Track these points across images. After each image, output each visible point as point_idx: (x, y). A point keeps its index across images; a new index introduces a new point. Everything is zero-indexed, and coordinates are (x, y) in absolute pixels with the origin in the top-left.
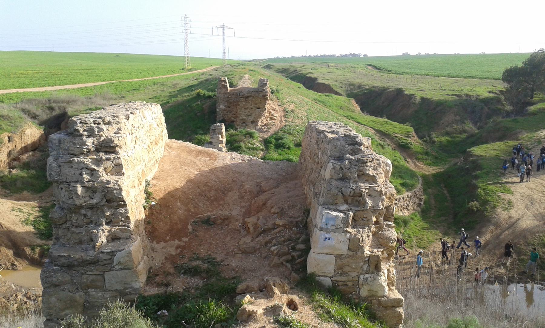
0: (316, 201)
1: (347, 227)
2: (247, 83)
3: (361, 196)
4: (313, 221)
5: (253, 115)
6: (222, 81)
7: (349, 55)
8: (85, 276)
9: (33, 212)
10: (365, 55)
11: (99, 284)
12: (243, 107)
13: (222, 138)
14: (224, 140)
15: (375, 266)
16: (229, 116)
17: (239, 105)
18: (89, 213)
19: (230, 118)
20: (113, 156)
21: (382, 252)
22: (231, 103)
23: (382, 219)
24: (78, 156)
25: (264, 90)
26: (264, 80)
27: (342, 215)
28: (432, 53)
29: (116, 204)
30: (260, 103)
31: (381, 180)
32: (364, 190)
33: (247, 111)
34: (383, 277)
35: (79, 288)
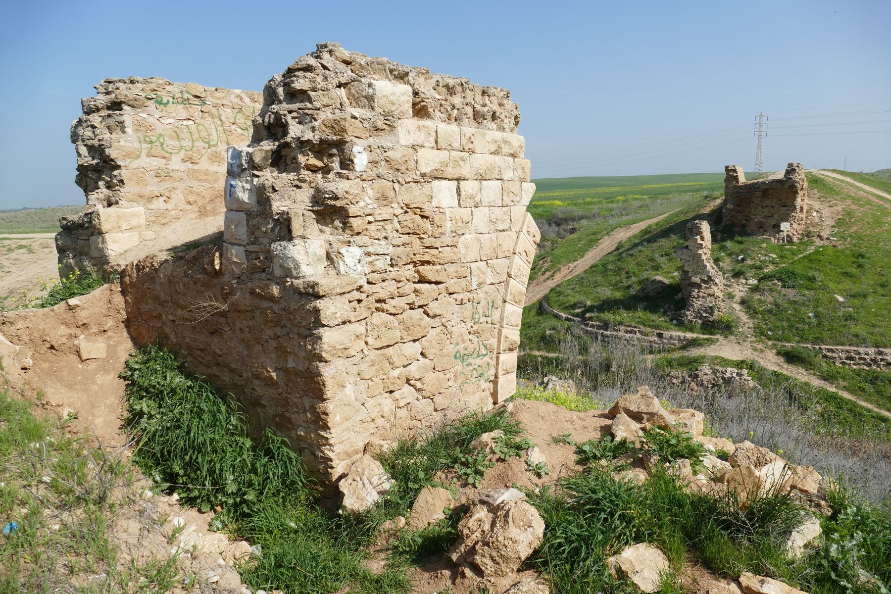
5: (776, 216)
13: (702, 239)
17: (753, 202)
33: (766, 211)
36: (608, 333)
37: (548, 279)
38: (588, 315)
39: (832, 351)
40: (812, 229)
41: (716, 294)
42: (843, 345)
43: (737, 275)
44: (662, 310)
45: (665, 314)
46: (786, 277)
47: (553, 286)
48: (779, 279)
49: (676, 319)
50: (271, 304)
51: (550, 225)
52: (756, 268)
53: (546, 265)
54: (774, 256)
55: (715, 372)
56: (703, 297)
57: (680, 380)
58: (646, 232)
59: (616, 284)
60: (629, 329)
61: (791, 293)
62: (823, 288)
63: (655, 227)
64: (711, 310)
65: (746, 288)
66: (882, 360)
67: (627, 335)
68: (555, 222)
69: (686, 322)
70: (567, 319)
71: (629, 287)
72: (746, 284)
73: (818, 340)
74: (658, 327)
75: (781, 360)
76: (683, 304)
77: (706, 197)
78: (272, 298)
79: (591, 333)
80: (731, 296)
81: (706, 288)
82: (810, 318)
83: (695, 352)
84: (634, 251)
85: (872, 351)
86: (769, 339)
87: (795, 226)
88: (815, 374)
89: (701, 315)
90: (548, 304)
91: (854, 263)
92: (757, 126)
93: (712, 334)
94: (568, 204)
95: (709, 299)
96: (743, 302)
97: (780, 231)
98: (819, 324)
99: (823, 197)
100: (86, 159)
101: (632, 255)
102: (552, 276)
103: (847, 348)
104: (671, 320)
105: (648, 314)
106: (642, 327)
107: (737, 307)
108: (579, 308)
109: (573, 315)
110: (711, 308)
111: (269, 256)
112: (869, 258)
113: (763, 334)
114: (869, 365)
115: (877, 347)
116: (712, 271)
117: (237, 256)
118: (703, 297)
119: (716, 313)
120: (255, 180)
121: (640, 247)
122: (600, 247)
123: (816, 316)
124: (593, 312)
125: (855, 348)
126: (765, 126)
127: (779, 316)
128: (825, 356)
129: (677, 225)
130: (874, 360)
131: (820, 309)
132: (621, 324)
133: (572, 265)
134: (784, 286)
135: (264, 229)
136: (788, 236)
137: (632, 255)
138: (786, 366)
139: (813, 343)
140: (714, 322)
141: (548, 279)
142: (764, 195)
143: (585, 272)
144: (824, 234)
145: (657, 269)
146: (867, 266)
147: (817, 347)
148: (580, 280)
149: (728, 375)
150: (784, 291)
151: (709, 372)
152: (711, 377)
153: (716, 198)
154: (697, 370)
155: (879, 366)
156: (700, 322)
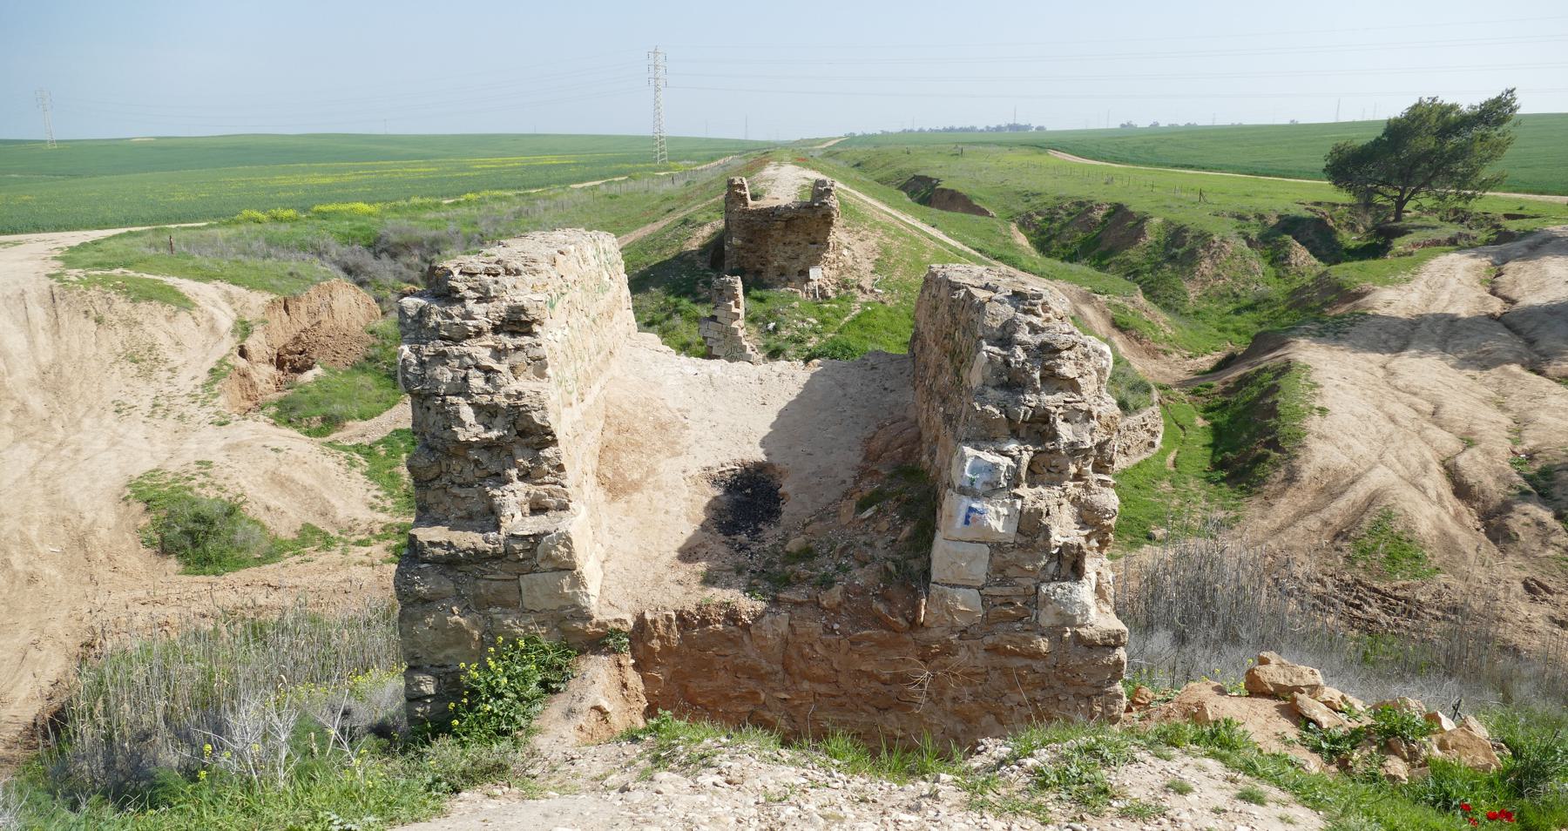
0: (949, 432)
1: (1017, 486)
2: (783, 187)
3: (1046, 421)
4: (944, 474)
5: (802, 258)
8: (481, 583)
10: (1039, 128)
11: (511, 598)
13: (737, 305)
14: (741, 311)
15: (1071, 565)
18: (484, 458)
20: (526, 340)
21: (1088, 538)
23: (1090, 468)
24: (457, 342)
26: (824, 182)
27: (1008, 461)
28: (1287, 122)
29: (536, 440)
31: (1089, 385)
32: (1053, 409)
33: (788, 249)
34: (1087, 588)
35: (472, 607)
40: (847, 276)
50: (1029, 662)
77: (685, 222)
78: (1036, 655)
87: (827, 270)
97: (808, 280)
100: (475, 430)
111: (1034, 600)
117: (963, 603)
120: (1019, 503)
126: (662, 71)
129: (653, 269)
135: (1030, 567)
144: (867, 283)
153: (701, 225)
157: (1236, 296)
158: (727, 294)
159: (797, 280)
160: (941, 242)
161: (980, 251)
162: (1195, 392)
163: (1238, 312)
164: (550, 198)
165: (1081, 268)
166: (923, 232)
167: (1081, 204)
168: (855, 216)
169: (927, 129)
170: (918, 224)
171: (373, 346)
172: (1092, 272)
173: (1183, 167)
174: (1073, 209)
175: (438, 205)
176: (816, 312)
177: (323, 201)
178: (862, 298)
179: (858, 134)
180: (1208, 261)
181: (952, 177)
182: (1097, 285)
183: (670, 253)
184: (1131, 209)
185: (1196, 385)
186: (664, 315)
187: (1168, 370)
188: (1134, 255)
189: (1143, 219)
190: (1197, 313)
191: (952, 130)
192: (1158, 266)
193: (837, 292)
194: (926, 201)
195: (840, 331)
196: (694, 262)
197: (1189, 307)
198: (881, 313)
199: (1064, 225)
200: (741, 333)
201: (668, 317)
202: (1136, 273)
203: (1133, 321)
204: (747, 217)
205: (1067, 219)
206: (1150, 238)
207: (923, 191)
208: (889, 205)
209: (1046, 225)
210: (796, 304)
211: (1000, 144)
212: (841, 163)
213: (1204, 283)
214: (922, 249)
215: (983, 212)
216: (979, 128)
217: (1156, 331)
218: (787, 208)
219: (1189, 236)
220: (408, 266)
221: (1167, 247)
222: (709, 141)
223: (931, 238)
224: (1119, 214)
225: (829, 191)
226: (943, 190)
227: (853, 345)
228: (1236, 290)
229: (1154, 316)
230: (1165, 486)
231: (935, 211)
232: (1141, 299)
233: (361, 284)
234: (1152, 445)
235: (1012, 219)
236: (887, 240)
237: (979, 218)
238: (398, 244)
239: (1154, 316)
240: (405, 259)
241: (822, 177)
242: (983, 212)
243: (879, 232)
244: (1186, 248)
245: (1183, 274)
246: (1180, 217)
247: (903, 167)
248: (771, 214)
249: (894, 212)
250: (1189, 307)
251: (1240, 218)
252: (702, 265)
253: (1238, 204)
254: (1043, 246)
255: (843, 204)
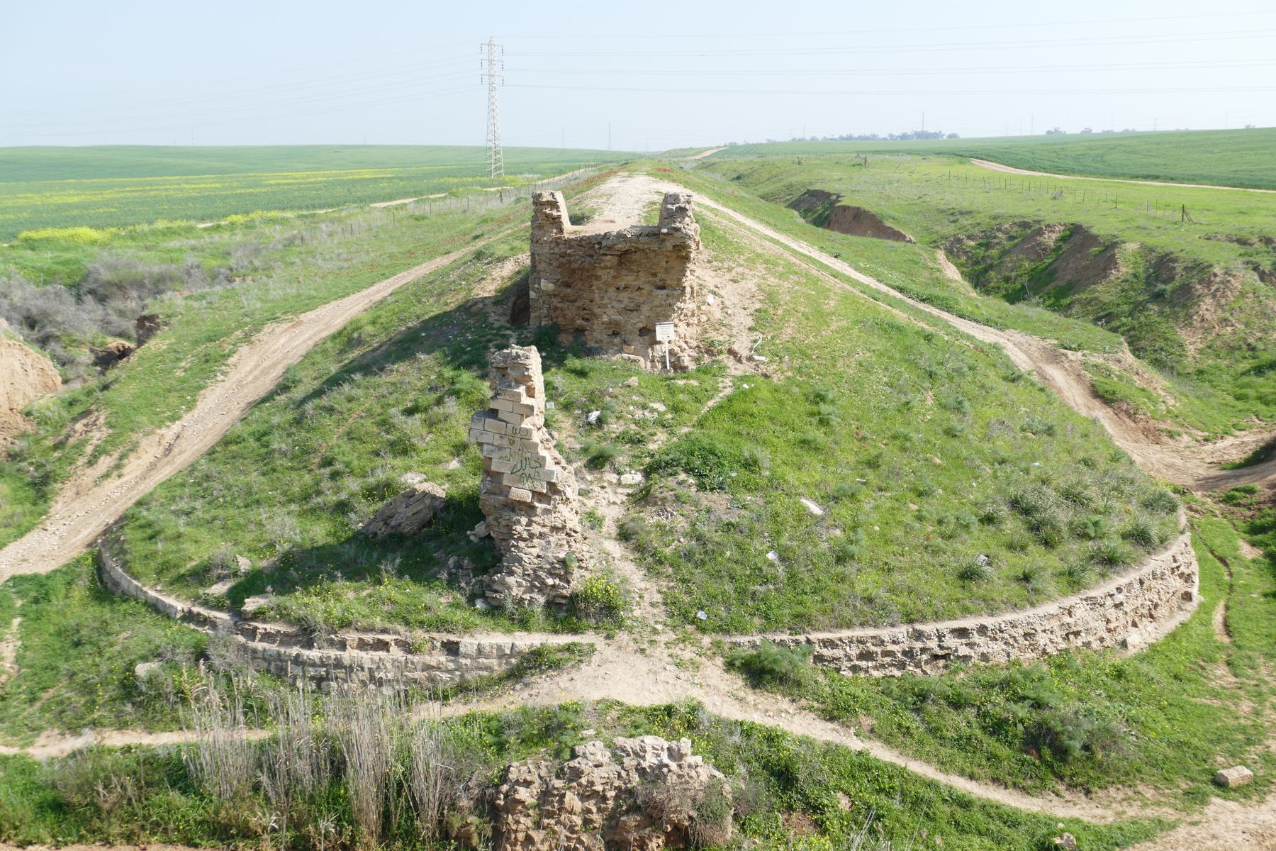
2: (622, 209)
5: (645, 309)
6: (543, 204)
7: (912, 136)
9: (213, 512)
12: (611, 285)
13: (531, 393)
16: (569, 314)
17: (598, 278)
19: (573, 320)
22: (574, 271)
25: (678, 230)
26: (675, 198)
28: (1242, 127)
30: (667, 271)
33: (624, 296)
36: (314, 654)
37: (106, 476)
38: (251, 604)
39: (830, 644)
40: (713, 335)
41: (569, 525)
42: (849, 626)
43: (597, 462)
44: (445, 576)
45: (452, 583)
46: (701, 464)
47: (125, 504)
48: (689, 470)
49: (483, 596)
51: (79, 299)
52: (631, 441)
53: (97, 436)
54: (662, 408)
55: (617, 755)
56: (541, 535)
57: (536, 788)
58: (348, 338)
59: (306, 498)
60: (369, 637)
61: (718, 501)
62: (775, 483)
63: (370, 329)
64: (563, 568)
65: (621, 496)
66: (923, 650)
67: (367, 657)
68: (92, 292)
69: (509, 605)
70: (189, 617)
71: (342, 508)
72: (619, 484)
73: (801, 621)
74: (442, 625)
75: (737, 682)
76: (490, 558)
77: (479, 255)
79: (266, 657)
80: (594, 521)
81: (547, 512)
82: (771, 565)
83: (547, 692)
84: (334, 398)
85: (902, 631)
86: (703, 630)
87: (682, 328)
88: (811, 709)
89: (543, 582)
90: (125, 565)
91: (812, 414)
92: (486, 63)
93: (575, 631)
94: (116, 237)
95: (553, 539)
96: (624, 535)
97: (654, 342)
98: (793, 578)
99: (716, 258)
101: (330, 410)
102: (118, 467)
103: (858, 633)
104: (471, 600)
105: (412, 589)
106: (401, 628)
107: (615, 549)
108: (221, 578)
109: (206, 604)
110: (563, 562)
112: (833, 402)
113: (688, 618)
114: (902, 666)
115: (911, 622)
116: (557, 469)
118: (541, 535)
119: (576, 573)
121: (346, 388)
122: (234, 376)
123: (783, 559)
124: (261, 592)
125: (870, 632)
127: (709, 566)
128: (819, 658)
129: (427, 325)
130: (909, 653)
131: (784, 540)
132: (345, 624)
133: (169, 432)
134: (701, 487)
136: (671, 353)
137: (330, 410)
138: (751, 697)
139: (793, 630)
140: (573, 598)
141: (106, 476)
142: (620, 264)
143: (211, 453)
144: (742, 347)
145: (405, 452)
146: (835, 421)
147: (802, 638)
148: (197, 481)
149: (650, 760)
150: (707, 499)
151: (604, 756)
152: (610, 770)
153: (501, 260)
154: (574, 756)
155: (918, 665)
156: (542, 600)
157: (1252, 348)
158: (511, 375)
159: (637, 342)
160: (849, 280)
161: (901, 290)
162: (1228, 499)
163: (1259, 371)
164: (340, 220)
165: (1034, 311)
166: (823, 266)
167: (1025, 225)
168: (720, 241)
169: (820, 137)
170: (816, 254)
171: (23, 435)
172: (1049, 315)
173: (1146, 177)
174: (1015, 231)
175: (190, 230)
176: (664, 393)
177: (32, 224)
178: (736, 370)
179: (740, 142)
180: (1208, 300)
181: (855, 192)
182: (1067, 337)
183: (453, 302)
184: (1094, 231)
185: (1228, 486)
186: (434, 396)
187: (1179, 462)
188: (1105, 292)
189: (1111, 247)
190: (1201, 372)
191: (849, 138)
192: (1138, 308)
193: (697, 360)
194: (823, 221)
195: (701, 424)
196: (486, 315)
197: (1189, 364)
198: (765, 393)
199: (1005, 253)
200: (537, 437)
201: (439, 402)
202: (1109, 317)
203: (1122, 389)
204: (562, 249)
205: (1007, 244)
206: (1124, 269)
207: (820, 209)
208: (775, 227)
209: (981, 252)
210: (634, 381)
211: (909, 153)
212: (718, 176)
213: (1207, 331)
214: (824, 293)
215: (898, 236)
216: (882, 136)
217: (1155, 403)
218: (620, 236)
219: (1179, 268)
220: (121, 313)
221: (1149, 281)
222: (564, 151)
223: (836, 275)
224: (1077, 239)
225: (683, 211)
226: (845, 208)
227: (720, 447)
228: (1251, 340)
229: (1149, 382)
230: (1221, 675)
231: (836, 235)
232: (1129, 358)
233: (43, 342)
234: (1187, 597)
235: (935, 244)
236: (772, 280)
237: (890, 242)
238: (109, 284)
239: (1149, 382)
240: (118, 303)
241: (672, 188)
242: (898, 236)
243: (761, 268)
244: (1177, 283)
245: (1177, 319)
246: (1165, 241)
247: (794, 179)
248: (595, 246)
249: (782, 238)
250: (1189, 364)
251: (1242, 242)
252: (497, 319)
253: (1234, 224)
254: (978, 280)
255: (707, 228)
